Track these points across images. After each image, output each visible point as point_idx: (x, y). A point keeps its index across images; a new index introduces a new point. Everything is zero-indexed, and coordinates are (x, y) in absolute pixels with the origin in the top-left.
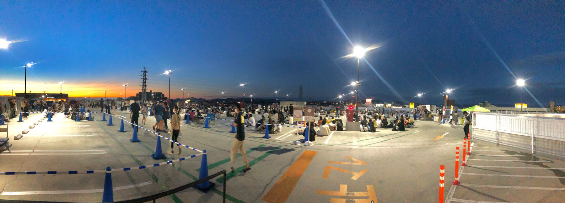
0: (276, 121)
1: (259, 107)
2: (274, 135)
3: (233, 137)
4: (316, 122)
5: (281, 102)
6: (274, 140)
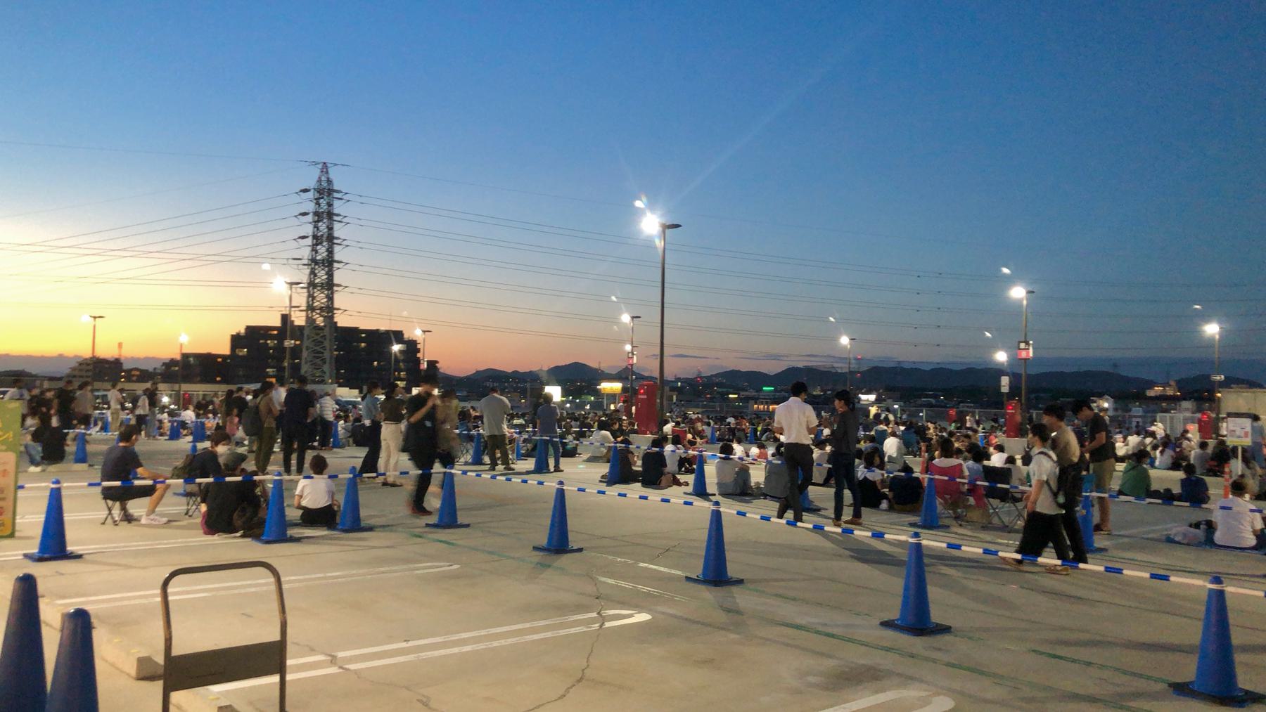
3: (87, 554)
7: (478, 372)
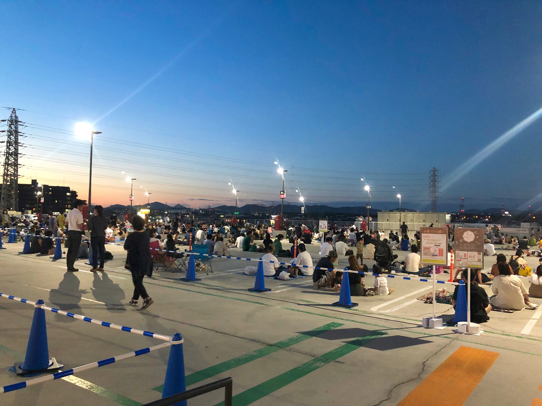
0: (371, 263)
1: (323, 226)
2: (366, 301)
4: (486, 270)
5: (379, 214)
6: (365, 312)
7: (112, 206)
